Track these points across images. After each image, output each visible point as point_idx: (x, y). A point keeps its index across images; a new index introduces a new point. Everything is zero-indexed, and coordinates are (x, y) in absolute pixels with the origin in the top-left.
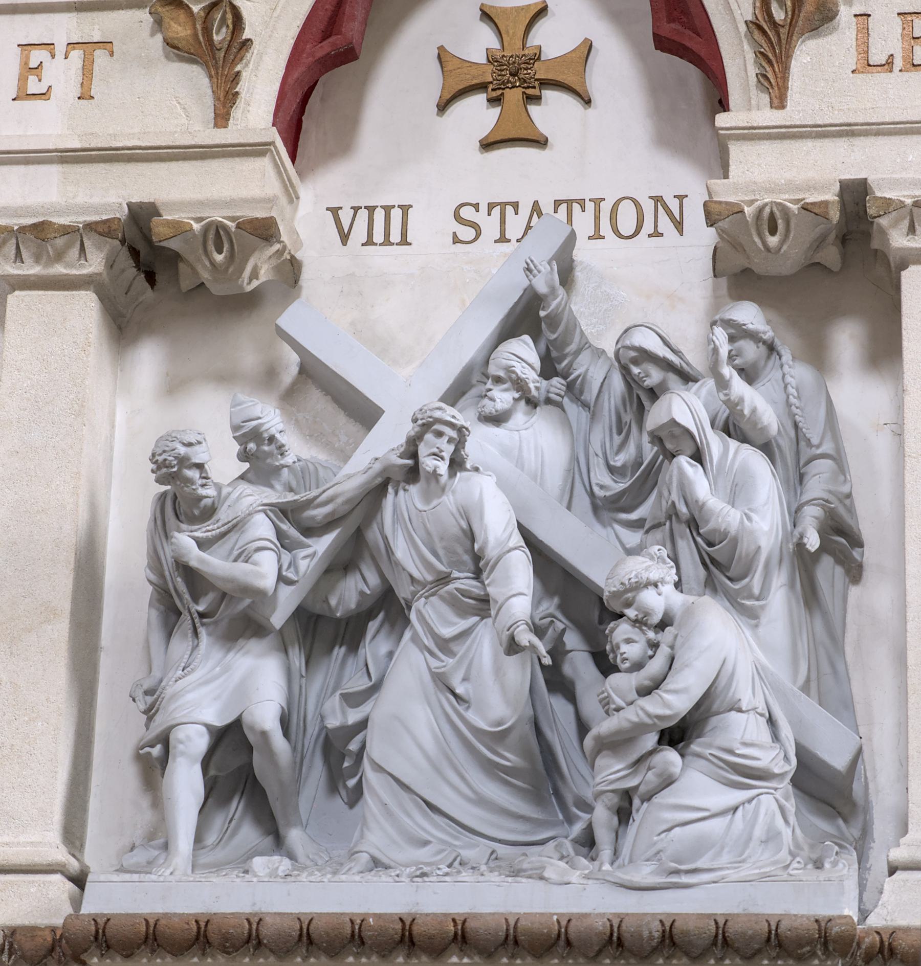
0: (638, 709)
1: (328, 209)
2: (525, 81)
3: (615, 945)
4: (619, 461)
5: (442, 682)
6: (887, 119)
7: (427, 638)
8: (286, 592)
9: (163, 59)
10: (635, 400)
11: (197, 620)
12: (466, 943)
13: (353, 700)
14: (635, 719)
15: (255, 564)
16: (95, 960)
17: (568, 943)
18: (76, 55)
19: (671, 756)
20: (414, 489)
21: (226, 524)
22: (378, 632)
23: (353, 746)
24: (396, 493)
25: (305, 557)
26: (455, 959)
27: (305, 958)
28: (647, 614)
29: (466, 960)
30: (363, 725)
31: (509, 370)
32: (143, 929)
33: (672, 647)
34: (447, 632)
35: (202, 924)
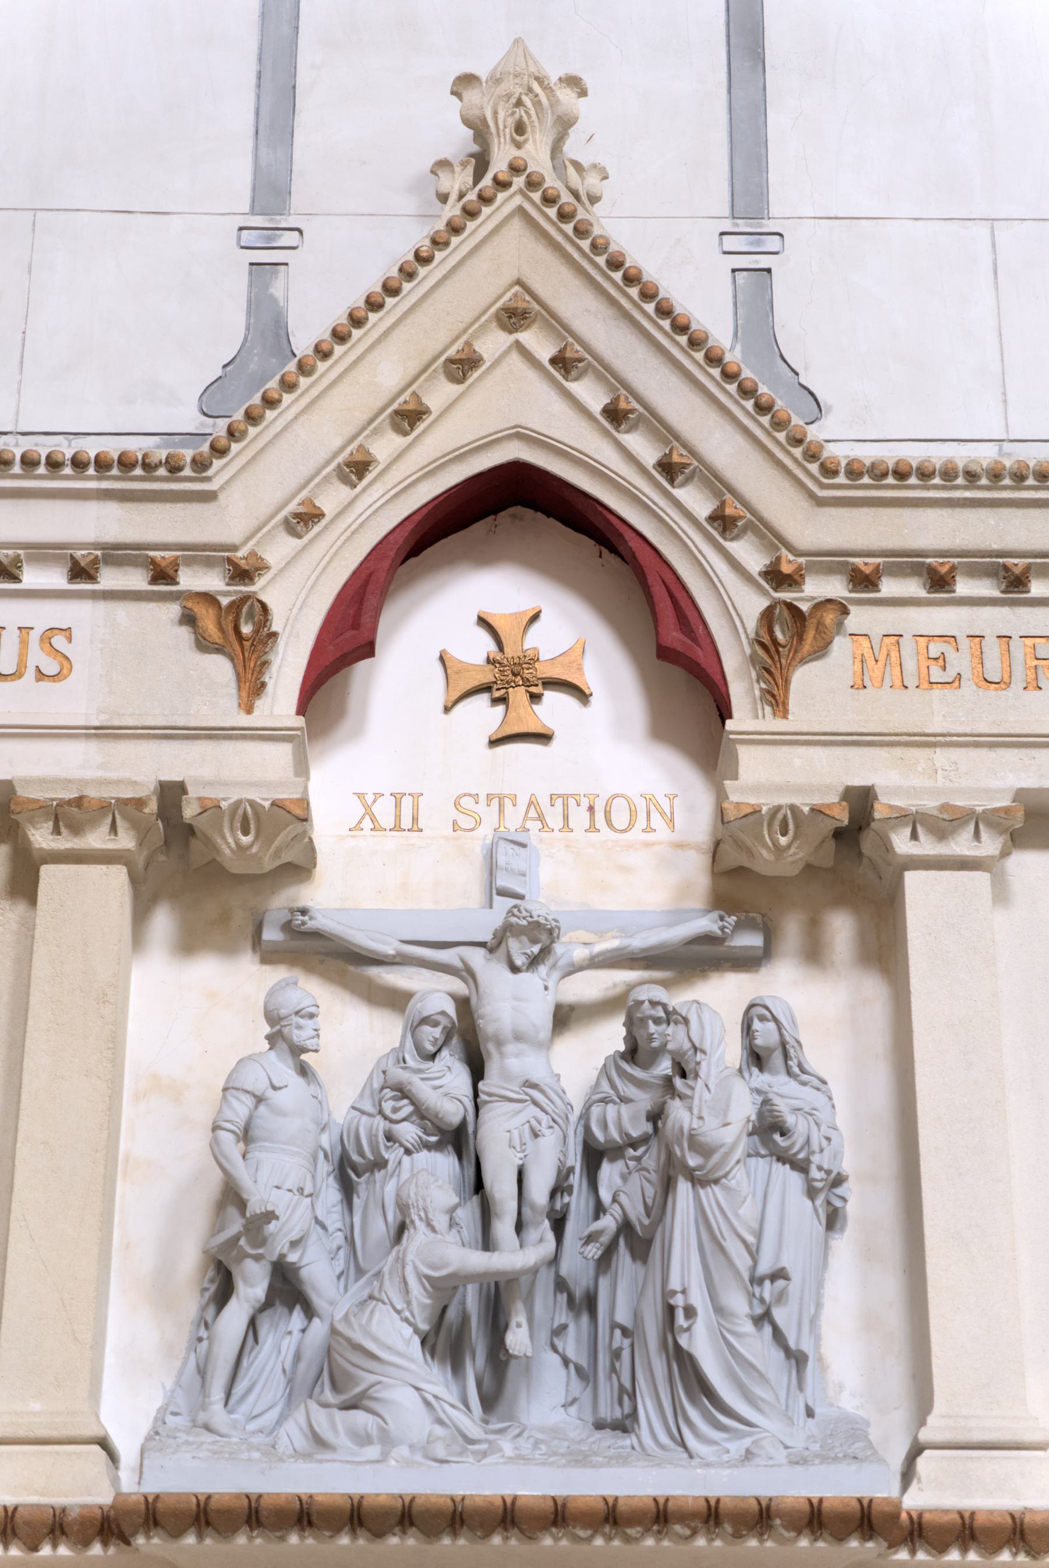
2: (528, 680)
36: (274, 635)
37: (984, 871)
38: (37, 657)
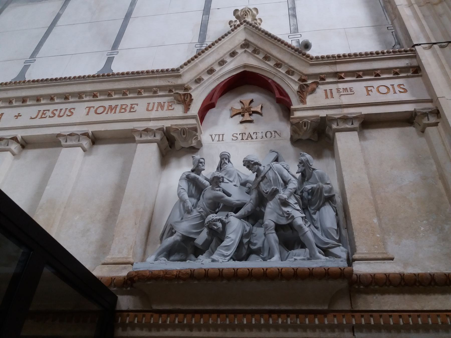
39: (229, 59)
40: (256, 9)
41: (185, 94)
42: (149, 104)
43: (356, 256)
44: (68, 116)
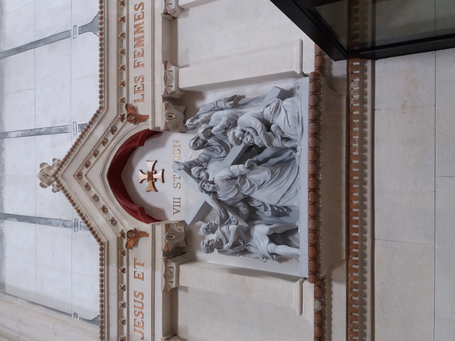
0: (260, 134)
1: (174, 215)
3: (316, 135)
4: (220, 151)
5: (260, 187)
6: (151, 93)
7: (250, 191)
8: (240, 224)
9: (138, 248)
10: (206, 147)
11: (245, 245)
12: (315, 174)
13: (266, 209)
14: (262, 135)
15: (231, 229)
16: (321, 275)
17: (316, 147)
18: (136, 266)
19: (273, 128)
20: (218, 193)
21: (223, 236)
22: (252, 203)
23: (276, 209)
24: (220, 197)
25: (232, 219)
26: (320, 178)
27: (320, 218)
28: (241, 135)
29: (321, 175)
30: (271, 206)
31: (197, 173)
32: (312, 261)
33: (247, 127)
34: (249, 185)
35: (311, 245)
36: (135, 229)
37: (179, 70)
38: (139, 299)
39: (93, 192)
40: (42, 165)
41: (128, 236)
42: (136, 306)
43: (298, 72)
44: (143, 298)
